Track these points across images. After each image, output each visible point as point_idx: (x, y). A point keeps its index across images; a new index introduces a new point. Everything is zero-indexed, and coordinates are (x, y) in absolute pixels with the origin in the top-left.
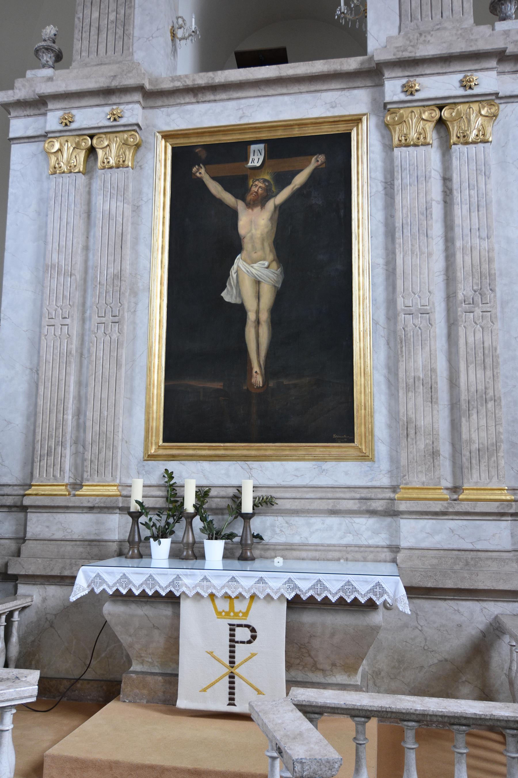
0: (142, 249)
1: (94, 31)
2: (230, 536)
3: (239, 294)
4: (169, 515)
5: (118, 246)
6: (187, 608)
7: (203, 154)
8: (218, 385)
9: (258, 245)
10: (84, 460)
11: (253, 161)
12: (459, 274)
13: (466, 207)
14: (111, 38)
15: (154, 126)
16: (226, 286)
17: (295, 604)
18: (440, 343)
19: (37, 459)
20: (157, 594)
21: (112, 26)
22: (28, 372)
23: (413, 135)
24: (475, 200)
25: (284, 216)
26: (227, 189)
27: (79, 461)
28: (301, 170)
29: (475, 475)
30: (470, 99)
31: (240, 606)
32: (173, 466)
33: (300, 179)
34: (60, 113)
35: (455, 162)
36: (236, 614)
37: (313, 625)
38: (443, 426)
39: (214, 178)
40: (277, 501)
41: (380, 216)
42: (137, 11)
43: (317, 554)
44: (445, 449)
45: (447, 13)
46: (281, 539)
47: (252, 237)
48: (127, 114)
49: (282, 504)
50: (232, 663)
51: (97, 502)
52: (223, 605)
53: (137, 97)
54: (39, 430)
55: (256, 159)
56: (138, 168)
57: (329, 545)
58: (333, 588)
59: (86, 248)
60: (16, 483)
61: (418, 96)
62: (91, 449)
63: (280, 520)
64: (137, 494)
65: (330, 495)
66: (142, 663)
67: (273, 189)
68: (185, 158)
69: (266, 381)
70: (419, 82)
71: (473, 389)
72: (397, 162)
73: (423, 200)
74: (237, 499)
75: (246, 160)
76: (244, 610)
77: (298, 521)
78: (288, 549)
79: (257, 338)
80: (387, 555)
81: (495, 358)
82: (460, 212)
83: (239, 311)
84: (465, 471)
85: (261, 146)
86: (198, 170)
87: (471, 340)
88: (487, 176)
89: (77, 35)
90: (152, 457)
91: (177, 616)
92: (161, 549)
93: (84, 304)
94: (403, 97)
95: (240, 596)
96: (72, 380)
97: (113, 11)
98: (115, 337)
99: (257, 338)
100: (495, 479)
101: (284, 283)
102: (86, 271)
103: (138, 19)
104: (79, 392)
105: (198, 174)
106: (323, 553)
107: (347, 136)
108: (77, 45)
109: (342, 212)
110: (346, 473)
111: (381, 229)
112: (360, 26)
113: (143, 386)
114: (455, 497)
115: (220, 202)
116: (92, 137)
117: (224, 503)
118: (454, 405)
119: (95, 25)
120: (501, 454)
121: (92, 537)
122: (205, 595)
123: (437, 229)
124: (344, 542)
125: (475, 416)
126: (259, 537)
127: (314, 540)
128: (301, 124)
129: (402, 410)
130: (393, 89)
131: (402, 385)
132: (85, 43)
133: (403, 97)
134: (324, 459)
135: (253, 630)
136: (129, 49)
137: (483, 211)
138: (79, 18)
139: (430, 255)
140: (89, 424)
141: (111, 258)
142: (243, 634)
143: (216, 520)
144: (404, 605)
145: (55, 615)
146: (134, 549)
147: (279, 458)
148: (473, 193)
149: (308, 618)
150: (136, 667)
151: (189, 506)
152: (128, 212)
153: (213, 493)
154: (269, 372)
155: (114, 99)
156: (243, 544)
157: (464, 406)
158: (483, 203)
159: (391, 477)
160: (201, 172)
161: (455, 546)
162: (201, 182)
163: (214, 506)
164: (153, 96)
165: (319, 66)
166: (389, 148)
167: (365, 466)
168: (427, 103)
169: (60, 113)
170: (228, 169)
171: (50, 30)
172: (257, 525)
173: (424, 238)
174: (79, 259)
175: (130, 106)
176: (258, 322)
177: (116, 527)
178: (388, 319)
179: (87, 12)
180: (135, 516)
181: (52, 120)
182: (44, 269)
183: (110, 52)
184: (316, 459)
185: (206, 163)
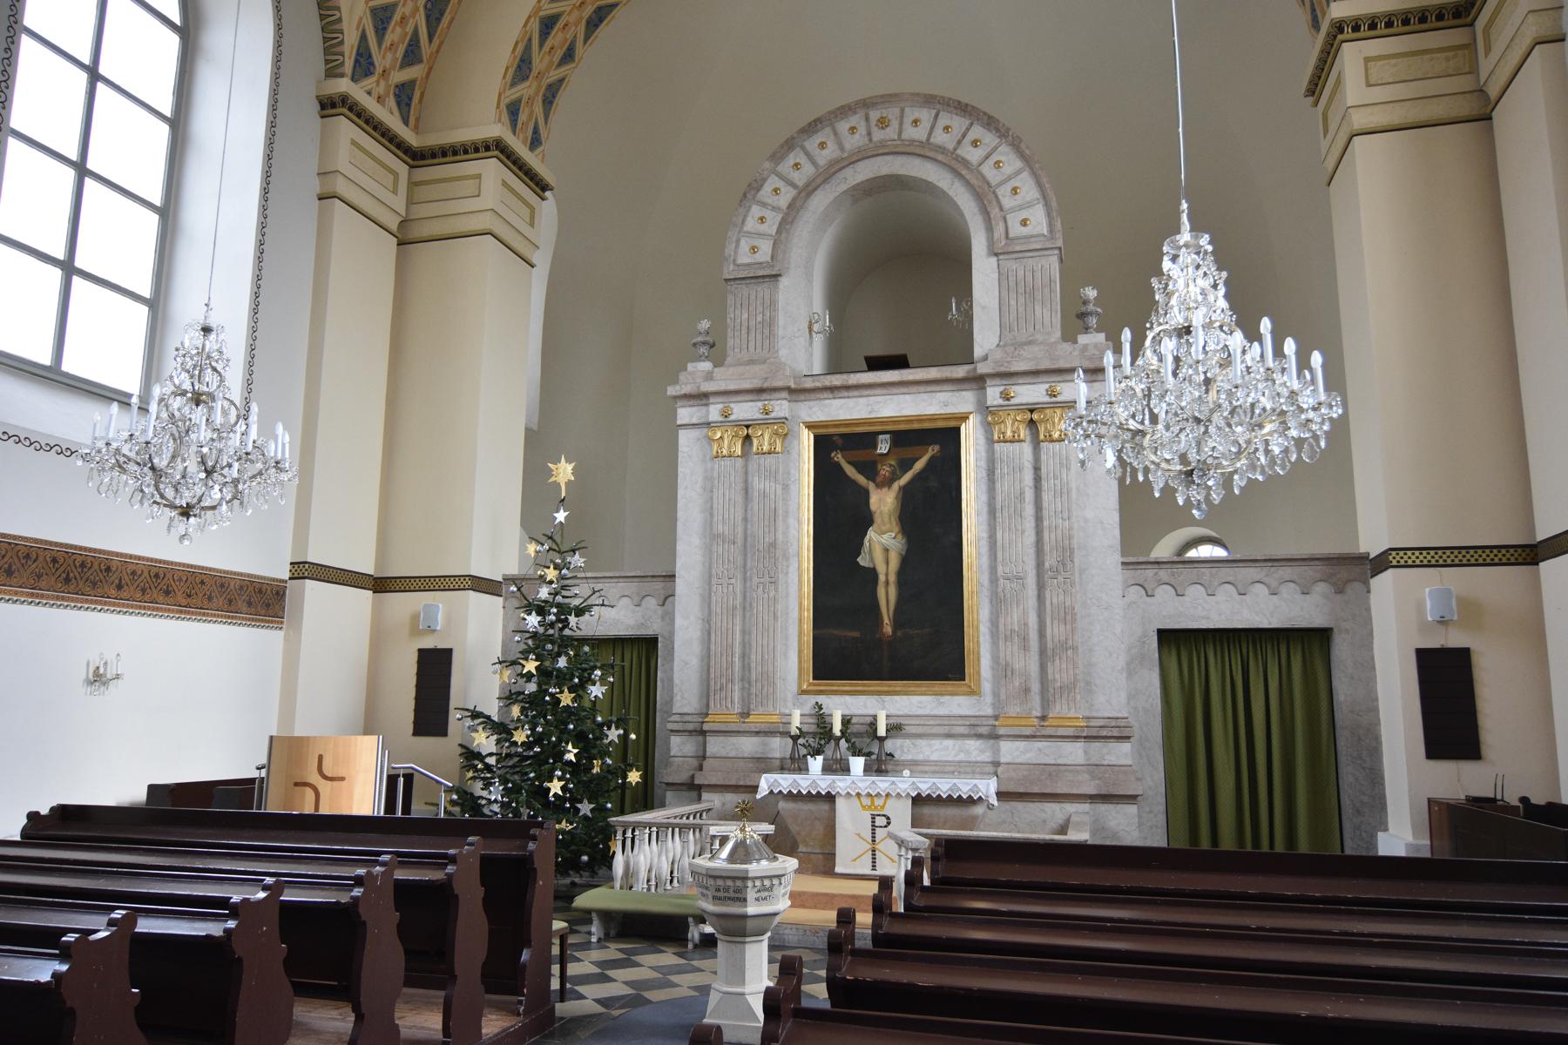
0: (792, 521)
1: (744, 331)
2: (868, 754)
3: (872, 559)
4: (820, 736)
6: (840, 804)
7: (840, 442)
10: (749, 694)
14: (759, 337)
17: (918, 800)
18: (1032, 602)
23: (1009, 434)
25: (906, 495)
29: (1058, 707)
30: (1055, 406)
31: (878, 802)
32: (821, 699)
33: (919, 465)
34: (720, 406)
35: (1043, 457)
38: (1034, 668)
41: (984, 498)
44: (1035, 687)
46: (909, 757)
49: (908, 729)
51: (763, 727)
52: (867, 801)
53: (784, 394)
55: (883, 447)
58: (944, 787)
59: (745, 520)
61: (1013, 401)
62: (755, 682)
63: (907, 742)
64: (796, 721)
70: (1014, 390)
72: (997, 455)
74: (873, 725)
75: (875, 447)
77: (922, 743)
78: (914, 765)
79: (887, 596)
80: (990, 769)
81: (1074, 615)
88: (1068, 469)
89: (730, 333)
90: (804, 692)
91: (833, 810)
92: (816, 764)
93: (745, 566)
94: (1001, 402)
95: (878, 795)
96: (738, 628)
99: (887, 596)
102: (746, 539)
103: (781, 320)
106: (941, 769)
107: (957, 430)
108: (730, 343)
111: (985, 509)
113: (796, 634)
115: (854, 482)
116: (747, 427)
117: (863, 729)
118: (1042, 652)
119: (745, 324)
123: (1029, 509)
126: (891, 755)
127: (934, 757)
128: (919, 419)
129: (1002, 655)
130: (993, 394)
131: (1002, 636)
133: (1001, 402)
139: (1023, 532)
142: (880, 821)
143: (858, 742)
144: (994, 801)
146: (796, 764)
147: (906, 693)
151: (837, 730)
152: (779, 492)
153: (854, 720)
154: (897, 624)
155: (765, 396)
156: (879, 760)
157: (1049, 653)
160: (838, 457)
162: (838, 465)
164: (797, 393)
165: (933, 373)
166: (990, 442)
167: (973, 699)
168: (1020, 408)
169: (720, 406)
170: (861, 455)
171: (705, 325)
172: (889, 745)
174: (740, 529)
176: (887, 583)
177: (779, 747)
180: (795, 738)
181: (714, 412)
182: (712, 537)
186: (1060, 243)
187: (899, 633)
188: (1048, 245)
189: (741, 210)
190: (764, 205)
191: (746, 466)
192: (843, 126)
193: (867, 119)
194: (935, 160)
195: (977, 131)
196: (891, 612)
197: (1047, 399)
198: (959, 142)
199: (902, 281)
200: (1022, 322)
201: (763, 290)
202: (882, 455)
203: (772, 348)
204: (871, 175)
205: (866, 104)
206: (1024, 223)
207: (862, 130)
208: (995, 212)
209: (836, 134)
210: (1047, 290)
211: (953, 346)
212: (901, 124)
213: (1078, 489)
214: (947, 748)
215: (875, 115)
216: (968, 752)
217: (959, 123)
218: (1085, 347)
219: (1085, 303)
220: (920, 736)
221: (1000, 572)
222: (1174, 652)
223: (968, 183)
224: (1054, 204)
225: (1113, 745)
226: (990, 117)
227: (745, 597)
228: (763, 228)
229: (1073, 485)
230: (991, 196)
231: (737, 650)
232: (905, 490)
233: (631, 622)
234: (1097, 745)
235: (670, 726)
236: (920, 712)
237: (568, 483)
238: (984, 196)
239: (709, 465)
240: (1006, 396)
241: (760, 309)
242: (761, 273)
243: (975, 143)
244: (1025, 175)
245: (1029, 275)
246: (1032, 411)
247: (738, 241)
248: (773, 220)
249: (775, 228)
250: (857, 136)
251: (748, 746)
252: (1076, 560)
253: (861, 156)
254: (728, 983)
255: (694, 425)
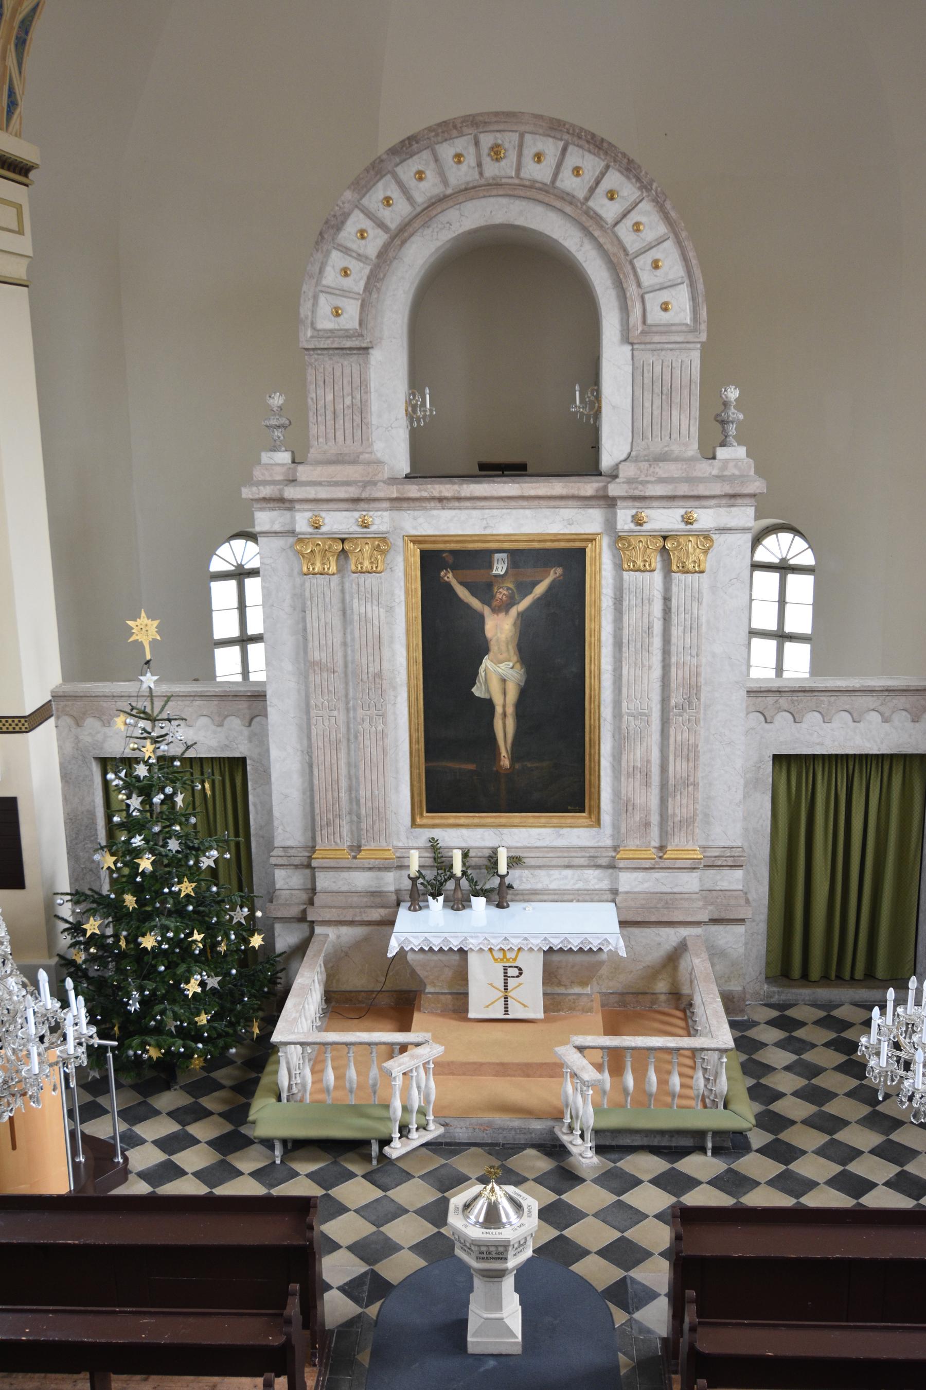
1: (330, 416)
3: (488, 690)
5: (377, 647)
6: (473, 959)
7: (450, 559)
8: (471, 767)
9: (503, 648)
10: (359, 829)
11: (497, 569)
12: (672, 685)
13: (681, 629)
14: (348, 425)
15: (402, 529)
16: (475, 683)
18: (655, 737)
19: (318, 829)
20: (451, 949)
21: (348, 412)
22: (299, 753)
23: (640, 563)
24: (688, 623)
25: (525, 623)
26: (474, 594)
27: (354, 828)
28: (541, 581)
29: (677, 840)
32: (437, 833)
35: (675, 589)
36: (508, 960)
37: (559, 962)
39: (462, 583)
40: (524, 860)
42: (373, 396)
43: (556, 897)
44: (655, 819)
45: (674, 436)
46: (528, 886)
47: (497, 640)
48: (377, 521)
50: (506, 989)
51: (373, 863)
54: (317, 806)
55: (500, 567)
56: (389, 570)
57: (565, 890)
59: (345, 644)
60: (299, 845)
63: (526, 873)
65: (566, 855)
66: (434, 986)
67: (516, 597)
68: (434, 561)
69: (512, 765)
71: (678, 776)
72: (626, 585)
73: (646, 620)
75: (490, 566)
76: (513, 957)
77: (542, 873)
79: (505, 728)
82: (676, 632)
83: (488, 705)
84: (669, 836)
85: (504, 555)
86: (446, 574)
87: (679, 738)
88: (700, 603)
89: (312, 419)
93: (347, 695)
95: (511, 949)
97: (348, 395)
98: (380, 728)
99: (505, 728)
100: (691, 842)
101: (527, 682)
102: (346, 666)
103: (375, 405)
104: (349, 772)
105: (446, 578)
107: (583, 551)
108: (313, 430)
109: (577, 622)
110: (579, 837)
112: (595, 422)
114: (661, 854)
115: (468, 606)
118: (664, 786)
120: (696, 824)
121: (374, 889)
122: (486, 949)
123: (657, 642)
124: (577, 887)
125: (679, 797)
127: (553, 886)
128: (541, 538)
129: (624, 792)
130: (624, 518)
131: (624, 772)
132: (322, 428)
134: (561, 826)
135: (520, 969)
136: (368, 440)
137: (695, 632)
138: (312, 399)
139: (650, 667)
140: (362, 801)
141: (371, 658)
142: (512, 972)
145: (349, 948)
148: (688, 616)
149: (556, 958)
150: (429, 989)
151: (458, 869)
153: (471, 854)
154: (514, 758)
155: (362, 505)
157: (671, 789)
158: (695, 626)
159: (613, 839)
160: (449, 577)
161: (659, 890)
162: (449, 586)
163: (473, 864)
165: (557, 487)
170: (471, 575)
171: (277, 400)
173: (645, 654)
175: (379, 513)
176: (504, 715)
178: (614, 717)
179: (320, 392)
181: (302, 522)
183: (349, 441)
184: (554, 826)
185: (454, 568)
186: (703, 337)
187: (517, 766)
188: (691, 337)
189: (319, 256)
190: (346, 251)
191: (342, 584)
192: (447, 151)
193: (477, 143)
194: (560, 210)
195: (614, 179)
196: (509, 734)
197: (682, 526)
198: (592, 190)
199: (509, 352)
200: (657, 428)
201: (350, 365)
202: (496, 576)
203: (365, 439)
204: (481, 223)
205: (475, 123)
206: (665, 307)
207: (470, 159)
208: (632, 290)
209: (436, 160)
210: (686, 392)
211: (576, 455)
212: (520, 155)
213: (708, 622)
214: (566, 878)
215: (487, 140)
216: (586, 881)
217: (591, 164)
218: (726, 462)
219: (726, 404)
220: (539, 867)
221: (624, 709)
222: (784, 768)
223: (600, 246)
224: (700, 286)
225: (726, 872)
226: (630, 161)
227: (348, 728)
228: (347, 283)
229: (703, 620)
230: (628, 268)
231: (344, 784)
232: (520, 615)
233: (213, 743)
234: (711, 872)
235: (273, 861)
236: (539, 844)
237: (153, 643)
238: (620, 266)
239: (298, 580)
240: (638, 521)
241: (347, 389)
242: (348, 344)
243: (611, 195)
244: (669, 245)
245: (667, 371)
246: (665, 538)
247: (316, 298)
248: (360, 272)
249: (362, 284)
250: (464, 167)
251: (361, 880)
252: (702, 700)
253: (468, 192)
254: (488, 1309)
255: (276, 533)
